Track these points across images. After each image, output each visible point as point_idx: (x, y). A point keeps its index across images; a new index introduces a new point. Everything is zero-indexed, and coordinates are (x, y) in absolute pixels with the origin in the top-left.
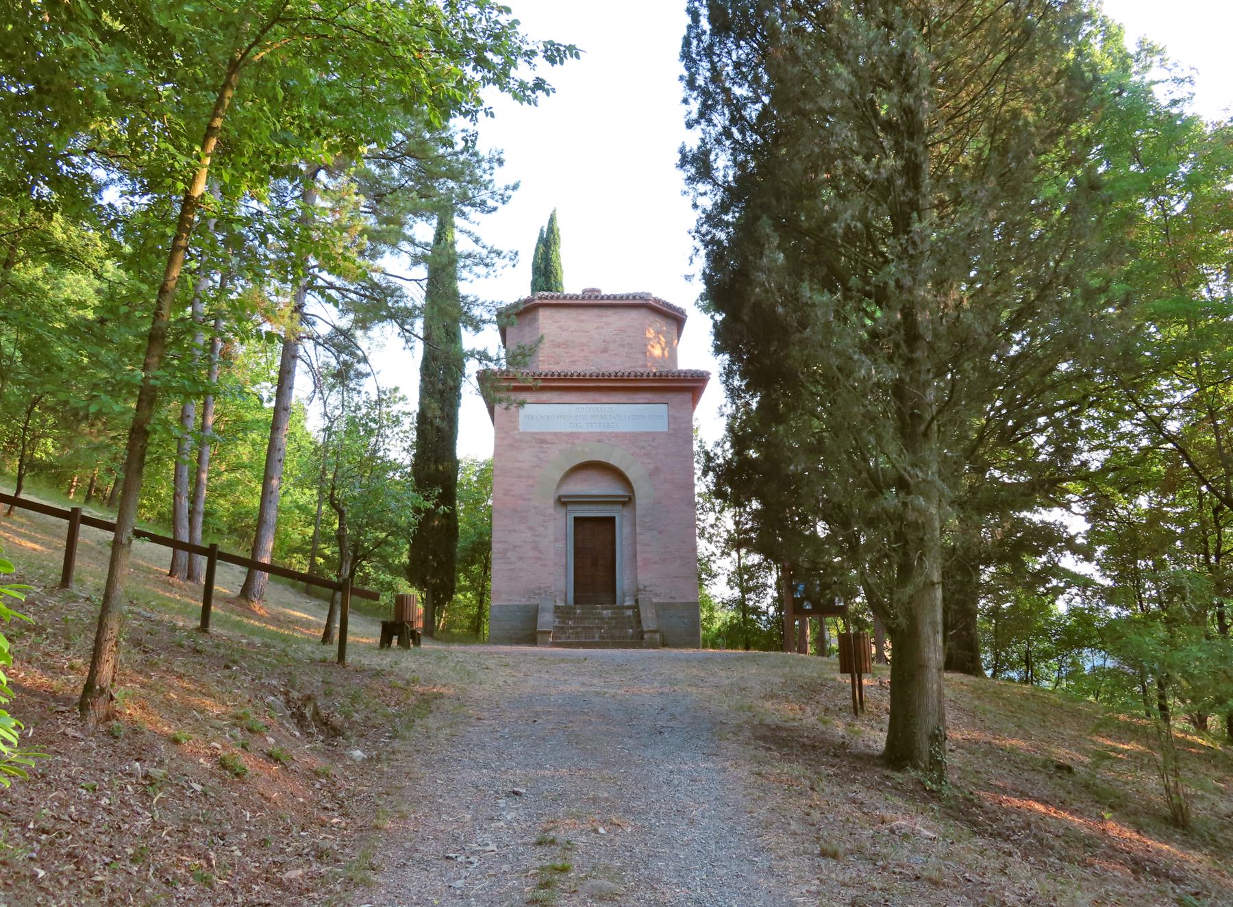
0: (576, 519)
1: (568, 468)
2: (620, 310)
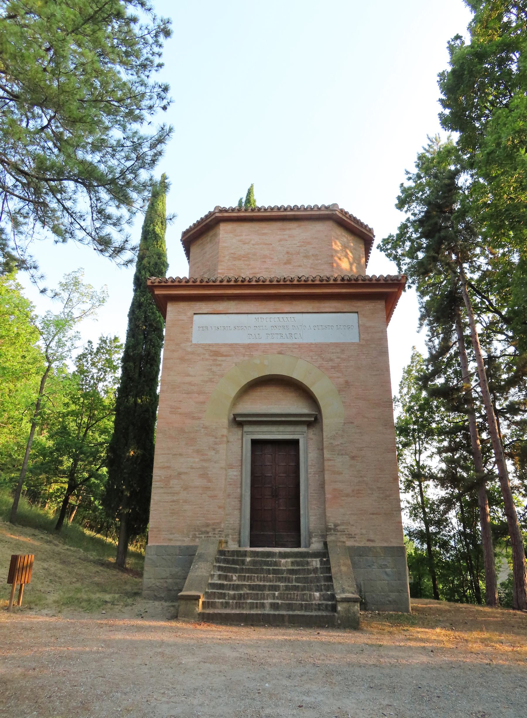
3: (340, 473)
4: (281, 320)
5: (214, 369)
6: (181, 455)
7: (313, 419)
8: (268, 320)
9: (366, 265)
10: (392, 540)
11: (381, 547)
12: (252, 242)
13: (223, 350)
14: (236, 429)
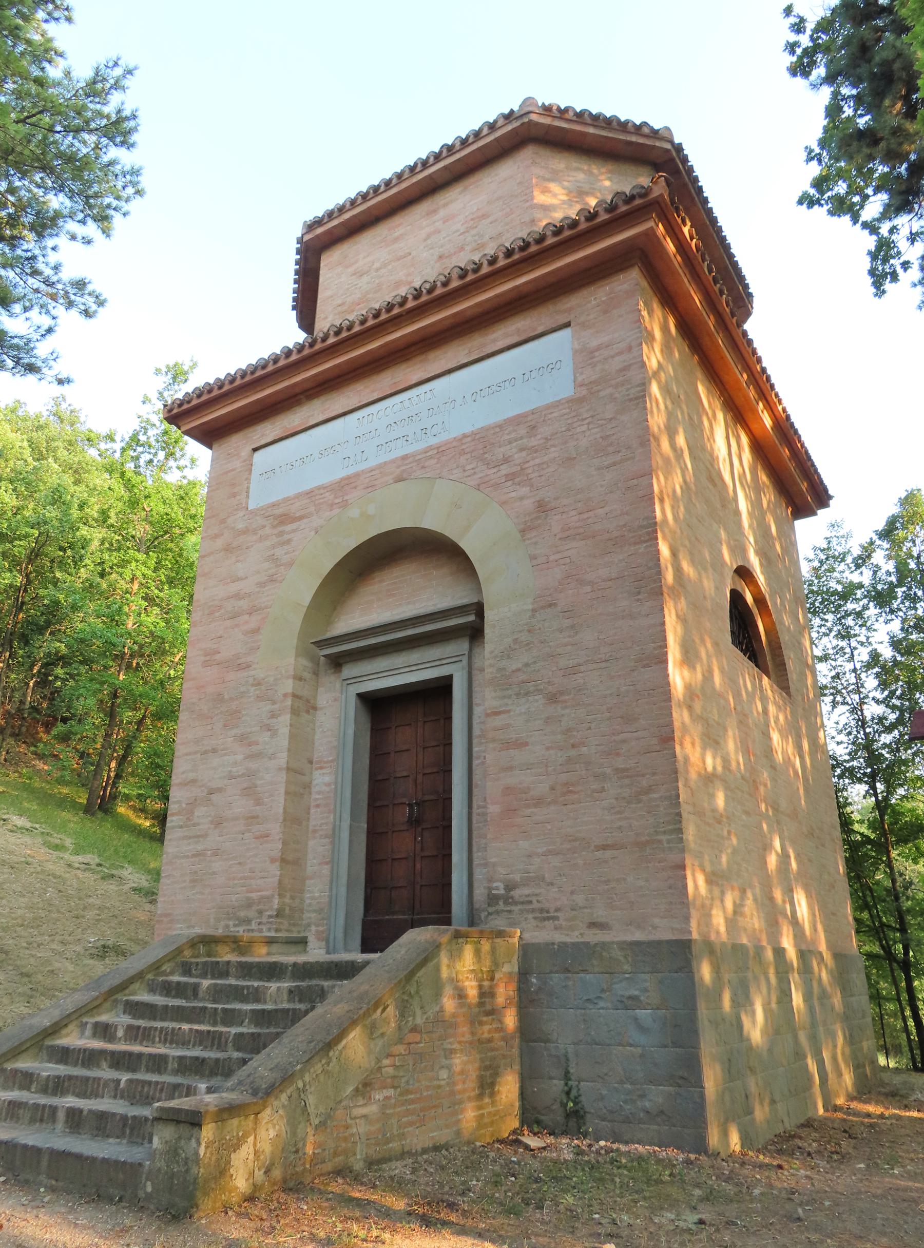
3: (520, 744)
5: (279, 552)
6: (214, 751)
10: (656, 921)
11: (623, 946)
12: (377, 265)
14: (332, 678)
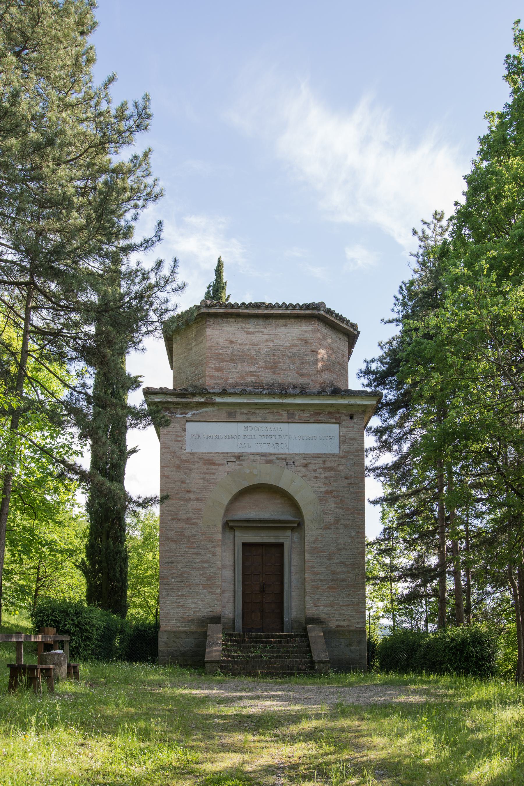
0: (244, 545)
1: (235, 491)
2: (289, 321)
4: (269, 429)
7: (296, 525)
8: (256, 429)
9: (349, 358)
13: (215, 458)
